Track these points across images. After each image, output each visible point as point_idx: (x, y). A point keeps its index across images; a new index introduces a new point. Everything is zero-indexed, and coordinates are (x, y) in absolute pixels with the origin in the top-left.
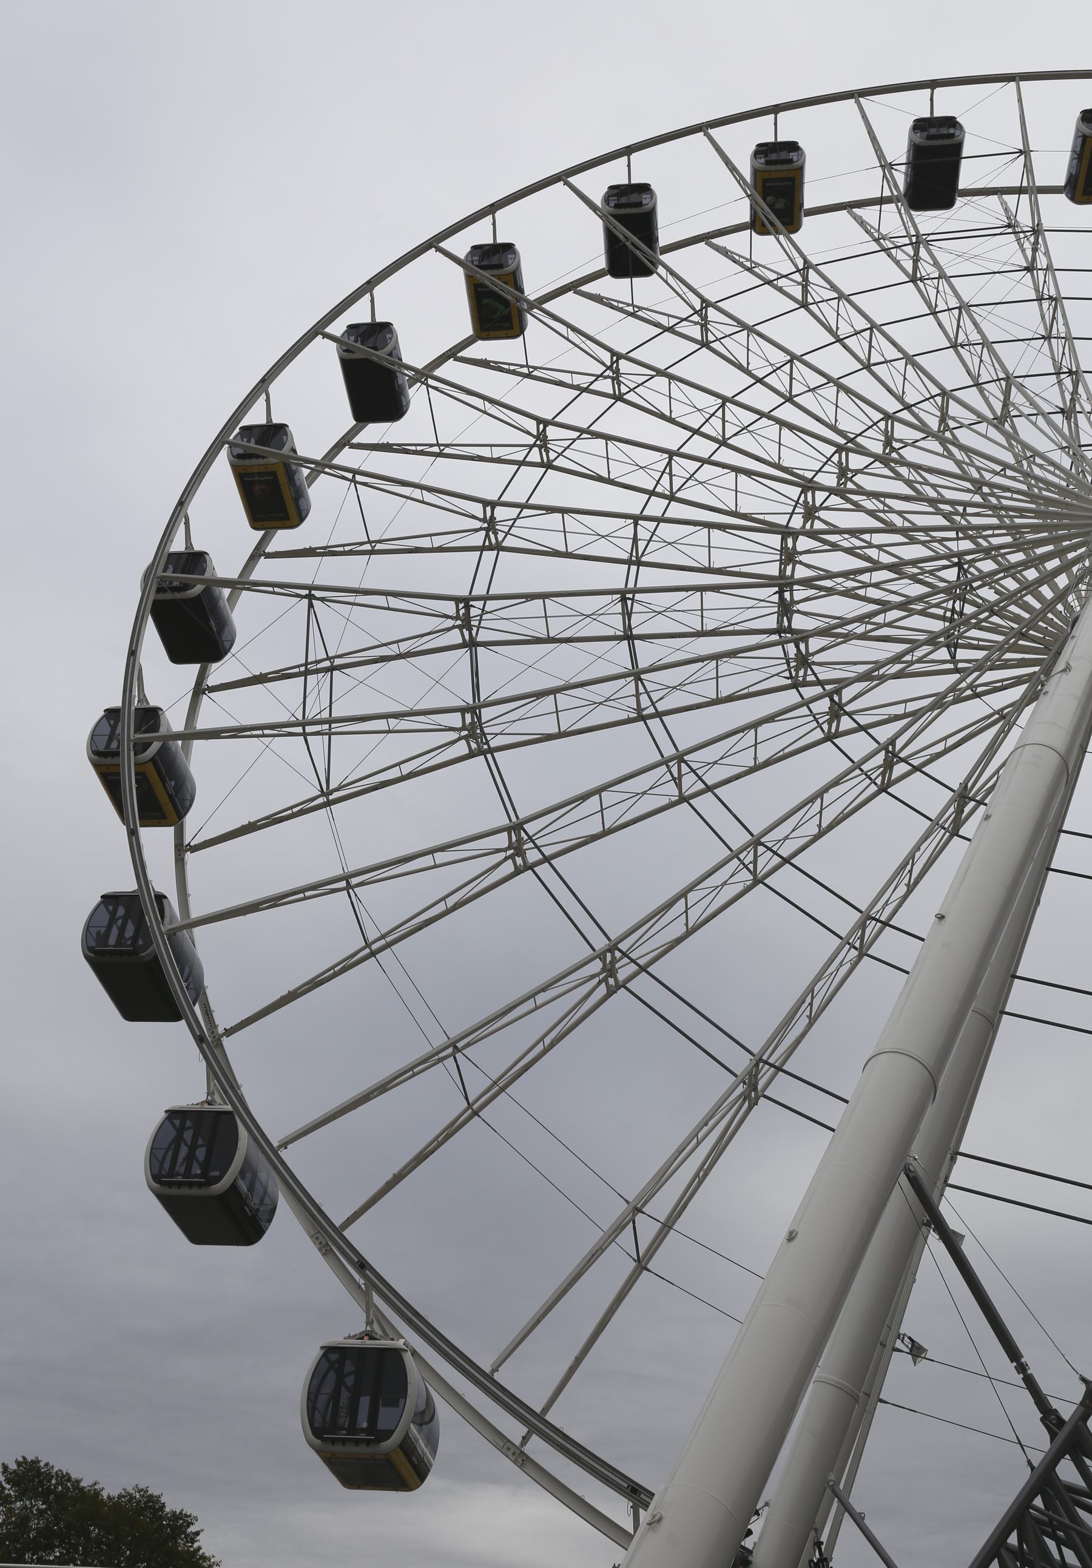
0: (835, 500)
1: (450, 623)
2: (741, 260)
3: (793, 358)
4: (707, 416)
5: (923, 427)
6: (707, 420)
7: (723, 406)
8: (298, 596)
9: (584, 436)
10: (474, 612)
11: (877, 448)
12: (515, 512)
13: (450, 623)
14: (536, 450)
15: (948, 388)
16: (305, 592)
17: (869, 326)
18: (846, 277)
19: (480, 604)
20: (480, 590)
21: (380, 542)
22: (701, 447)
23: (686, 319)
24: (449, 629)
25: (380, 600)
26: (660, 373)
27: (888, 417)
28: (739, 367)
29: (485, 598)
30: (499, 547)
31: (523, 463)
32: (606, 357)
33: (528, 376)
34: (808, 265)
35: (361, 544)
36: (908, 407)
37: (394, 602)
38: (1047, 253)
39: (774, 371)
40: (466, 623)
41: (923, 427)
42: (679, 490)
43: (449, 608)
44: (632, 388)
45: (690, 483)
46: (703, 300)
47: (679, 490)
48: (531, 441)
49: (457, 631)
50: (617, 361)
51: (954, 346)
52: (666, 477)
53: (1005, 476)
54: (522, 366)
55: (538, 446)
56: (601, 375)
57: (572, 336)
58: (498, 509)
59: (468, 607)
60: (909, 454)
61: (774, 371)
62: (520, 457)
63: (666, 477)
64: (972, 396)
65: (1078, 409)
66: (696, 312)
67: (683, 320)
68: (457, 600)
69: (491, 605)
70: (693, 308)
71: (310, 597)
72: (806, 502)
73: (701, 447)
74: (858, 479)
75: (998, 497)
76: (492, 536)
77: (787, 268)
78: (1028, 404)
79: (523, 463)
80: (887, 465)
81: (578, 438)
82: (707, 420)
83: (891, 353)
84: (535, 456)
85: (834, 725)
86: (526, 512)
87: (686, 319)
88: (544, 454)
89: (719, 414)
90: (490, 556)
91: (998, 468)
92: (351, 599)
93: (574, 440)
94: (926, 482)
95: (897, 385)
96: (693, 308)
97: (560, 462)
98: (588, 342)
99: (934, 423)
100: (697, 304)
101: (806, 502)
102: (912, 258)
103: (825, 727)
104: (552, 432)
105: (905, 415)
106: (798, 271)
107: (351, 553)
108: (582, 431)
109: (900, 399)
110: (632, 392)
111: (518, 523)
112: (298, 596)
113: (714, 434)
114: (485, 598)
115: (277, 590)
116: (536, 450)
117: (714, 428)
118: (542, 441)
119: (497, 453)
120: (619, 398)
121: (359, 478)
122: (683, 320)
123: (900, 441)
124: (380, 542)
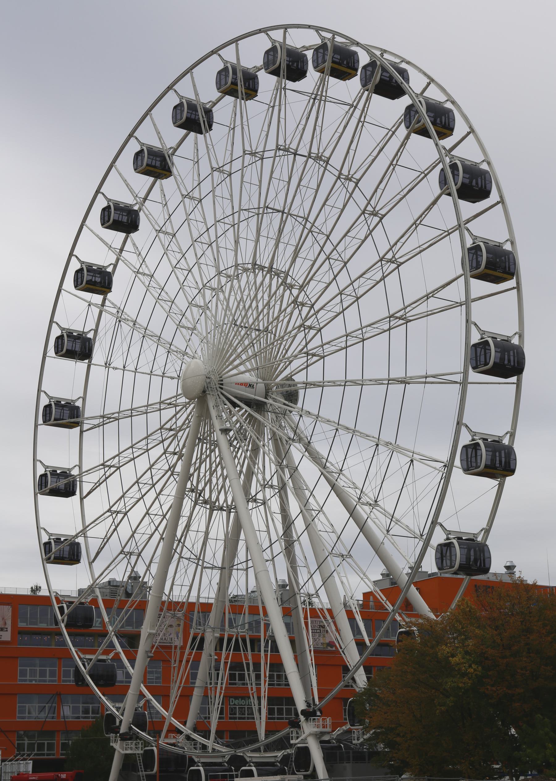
0: (280, 281)
1: (321, 151)
2: (95, 486)
3: (137, 482)
4: (316, 241)
5: (306, 319)
6: (317, 242)
7: (343, 261)
8: (355, 101)
9: (369, 231)
10: (322, 163)
11: (300, 299)
12: (350, 190)
13: (321, 151)
14: (372, 210)
15: (159, 427)
16: (355, 104)
17: (137, 484)
18: (111, 452)
19: (324, 165)
20: (329, 167)
21: (394, 169)
22: (328, 248)
23: (114, 520)
24: (318, 149)
25: (375, 154)
26: (383, 278)
27: (312, 306)
28: (364, 274)
29: (325, 169)
30: (339, 178)
31: (369, 203)
32: (122, 556)
33: (415, 223)
34: (103, 465)
35: (397, 161)
36: (170, 469)
37: (371, 158)
38: (113, 414)
39: (332, 269)
40: (318, 158)
41: (306, 319)
42: (312, 234)
43: (327, 154)
44: (474, 305)
45: (314, 239)
46: (108, 511)
47: (312, 234)
48: (377, 209)
49: (317, 152)
50: (124, 552)
51: (147, 450)
52: (318, 231)
53: (283, 350)
54: (421, 221)
55: (373, 211)
56: (129, 560)
57: (110, 568)
58: (354, 184)
59: (324, 161)
60: (296, 312)
61: (332, 269)
62: (372, 203)
63: (318, 231)
64: (166, 443)
65: (175, 402)
66: (112, 515)
67: (114, 521)
68: (329, 159)
69: (322, 169)
70: (124, 558)
71: (352, 106)
72: (201, 503)
73: (328, 248)
74: (288, 291)
75: (263, 337)
76: (344, 177)
77: (110, 520)
78: (171, 421)
79: (369, 203)
80: (293, 302)
81: (369, 229)
82: (317, 242)
83: (148, 474)
84: (369, 208)
85: (259, 501)
86: (348, 195)
87: (114, 520)
88: (369, 212)
89: (340, 259)
90: (337, 173)
91: (286, 347)
92: (380, 145)
93: (369, 227)
94: (285, 317)
95: (162, 472)
96: (110, 515)
97: (362, 217)
98: (115, 561)
99: (308, 323)
100: (109, 514)
101: (201, 503)
102: (110, 468)
103: (259, 504)
104: (376, 219)
105: (312, 312)
106: (104, 468)
107: (421, 216)
108: (371, 232)
109: (167, 471)
110: (474, 305)
111: (345, 190)
112: (355, 101)
113: (333, 254)
114: (325, 169)
115: (360, 94)
116: (372, 210)
117: (335, 255)
118: (374, 214)
119: (379, 191)
120: (381, 260)
121: (423, 175)
122: (114, 521)
123: (302, 309)
124: (394, 169)
